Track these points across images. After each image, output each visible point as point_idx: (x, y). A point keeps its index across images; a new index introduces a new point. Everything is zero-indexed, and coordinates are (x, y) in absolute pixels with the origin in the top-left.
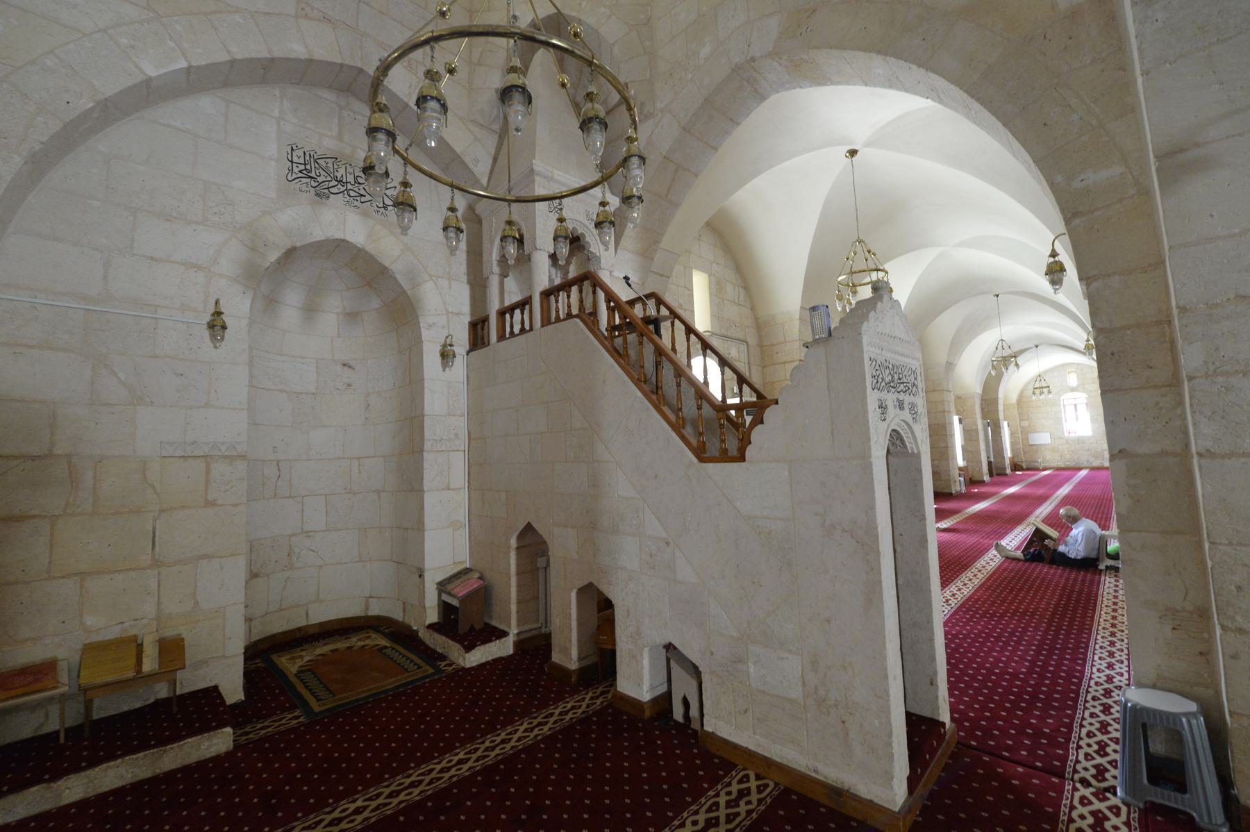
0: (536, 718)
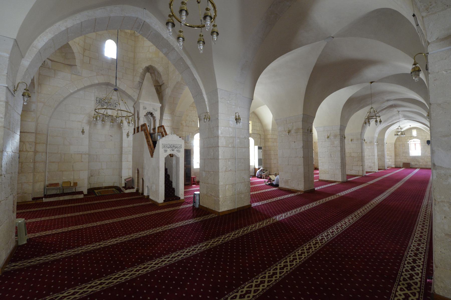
0: (192, 248)
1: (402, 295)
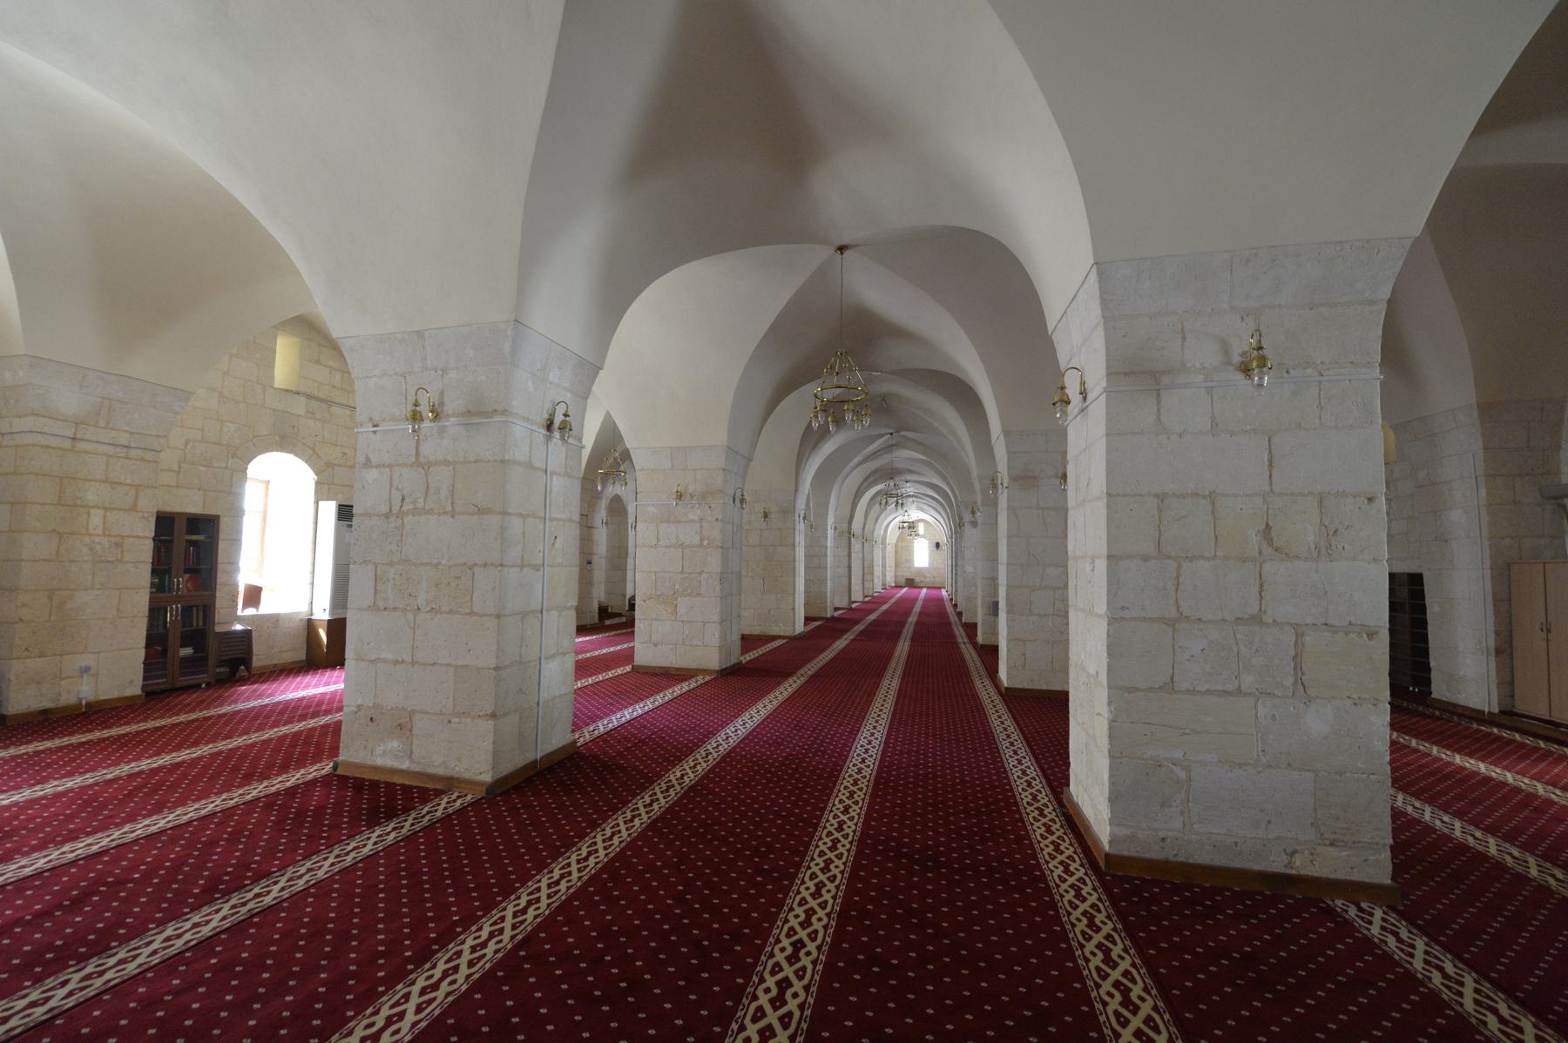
1: (1064, 850)
